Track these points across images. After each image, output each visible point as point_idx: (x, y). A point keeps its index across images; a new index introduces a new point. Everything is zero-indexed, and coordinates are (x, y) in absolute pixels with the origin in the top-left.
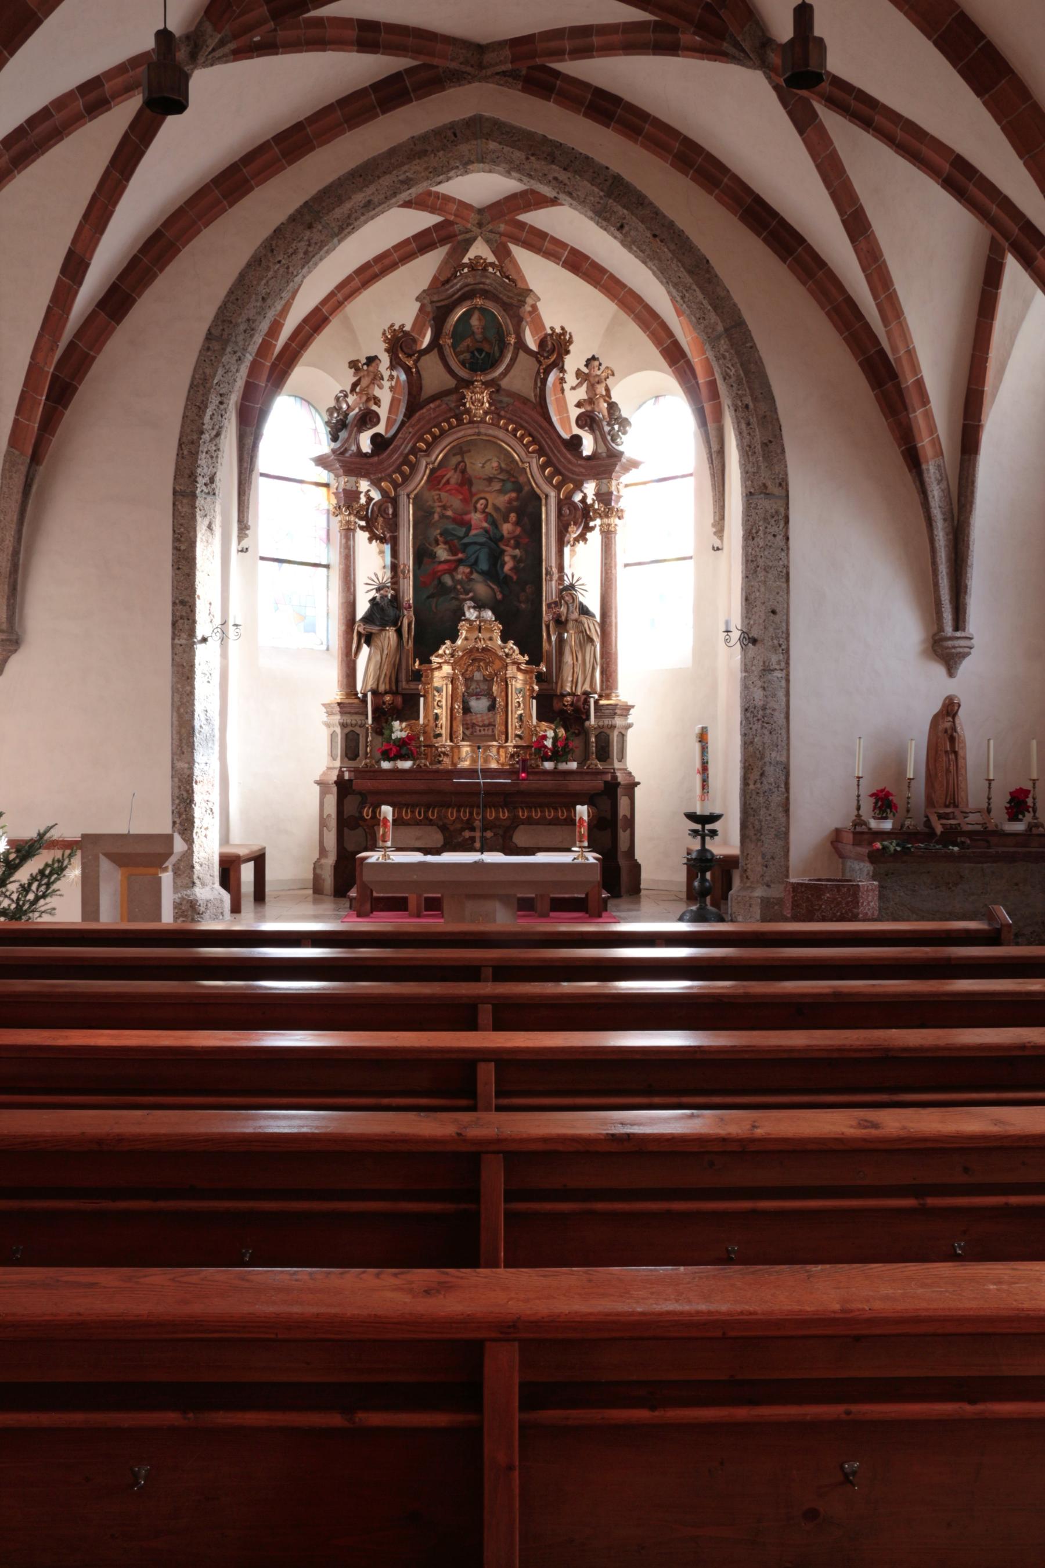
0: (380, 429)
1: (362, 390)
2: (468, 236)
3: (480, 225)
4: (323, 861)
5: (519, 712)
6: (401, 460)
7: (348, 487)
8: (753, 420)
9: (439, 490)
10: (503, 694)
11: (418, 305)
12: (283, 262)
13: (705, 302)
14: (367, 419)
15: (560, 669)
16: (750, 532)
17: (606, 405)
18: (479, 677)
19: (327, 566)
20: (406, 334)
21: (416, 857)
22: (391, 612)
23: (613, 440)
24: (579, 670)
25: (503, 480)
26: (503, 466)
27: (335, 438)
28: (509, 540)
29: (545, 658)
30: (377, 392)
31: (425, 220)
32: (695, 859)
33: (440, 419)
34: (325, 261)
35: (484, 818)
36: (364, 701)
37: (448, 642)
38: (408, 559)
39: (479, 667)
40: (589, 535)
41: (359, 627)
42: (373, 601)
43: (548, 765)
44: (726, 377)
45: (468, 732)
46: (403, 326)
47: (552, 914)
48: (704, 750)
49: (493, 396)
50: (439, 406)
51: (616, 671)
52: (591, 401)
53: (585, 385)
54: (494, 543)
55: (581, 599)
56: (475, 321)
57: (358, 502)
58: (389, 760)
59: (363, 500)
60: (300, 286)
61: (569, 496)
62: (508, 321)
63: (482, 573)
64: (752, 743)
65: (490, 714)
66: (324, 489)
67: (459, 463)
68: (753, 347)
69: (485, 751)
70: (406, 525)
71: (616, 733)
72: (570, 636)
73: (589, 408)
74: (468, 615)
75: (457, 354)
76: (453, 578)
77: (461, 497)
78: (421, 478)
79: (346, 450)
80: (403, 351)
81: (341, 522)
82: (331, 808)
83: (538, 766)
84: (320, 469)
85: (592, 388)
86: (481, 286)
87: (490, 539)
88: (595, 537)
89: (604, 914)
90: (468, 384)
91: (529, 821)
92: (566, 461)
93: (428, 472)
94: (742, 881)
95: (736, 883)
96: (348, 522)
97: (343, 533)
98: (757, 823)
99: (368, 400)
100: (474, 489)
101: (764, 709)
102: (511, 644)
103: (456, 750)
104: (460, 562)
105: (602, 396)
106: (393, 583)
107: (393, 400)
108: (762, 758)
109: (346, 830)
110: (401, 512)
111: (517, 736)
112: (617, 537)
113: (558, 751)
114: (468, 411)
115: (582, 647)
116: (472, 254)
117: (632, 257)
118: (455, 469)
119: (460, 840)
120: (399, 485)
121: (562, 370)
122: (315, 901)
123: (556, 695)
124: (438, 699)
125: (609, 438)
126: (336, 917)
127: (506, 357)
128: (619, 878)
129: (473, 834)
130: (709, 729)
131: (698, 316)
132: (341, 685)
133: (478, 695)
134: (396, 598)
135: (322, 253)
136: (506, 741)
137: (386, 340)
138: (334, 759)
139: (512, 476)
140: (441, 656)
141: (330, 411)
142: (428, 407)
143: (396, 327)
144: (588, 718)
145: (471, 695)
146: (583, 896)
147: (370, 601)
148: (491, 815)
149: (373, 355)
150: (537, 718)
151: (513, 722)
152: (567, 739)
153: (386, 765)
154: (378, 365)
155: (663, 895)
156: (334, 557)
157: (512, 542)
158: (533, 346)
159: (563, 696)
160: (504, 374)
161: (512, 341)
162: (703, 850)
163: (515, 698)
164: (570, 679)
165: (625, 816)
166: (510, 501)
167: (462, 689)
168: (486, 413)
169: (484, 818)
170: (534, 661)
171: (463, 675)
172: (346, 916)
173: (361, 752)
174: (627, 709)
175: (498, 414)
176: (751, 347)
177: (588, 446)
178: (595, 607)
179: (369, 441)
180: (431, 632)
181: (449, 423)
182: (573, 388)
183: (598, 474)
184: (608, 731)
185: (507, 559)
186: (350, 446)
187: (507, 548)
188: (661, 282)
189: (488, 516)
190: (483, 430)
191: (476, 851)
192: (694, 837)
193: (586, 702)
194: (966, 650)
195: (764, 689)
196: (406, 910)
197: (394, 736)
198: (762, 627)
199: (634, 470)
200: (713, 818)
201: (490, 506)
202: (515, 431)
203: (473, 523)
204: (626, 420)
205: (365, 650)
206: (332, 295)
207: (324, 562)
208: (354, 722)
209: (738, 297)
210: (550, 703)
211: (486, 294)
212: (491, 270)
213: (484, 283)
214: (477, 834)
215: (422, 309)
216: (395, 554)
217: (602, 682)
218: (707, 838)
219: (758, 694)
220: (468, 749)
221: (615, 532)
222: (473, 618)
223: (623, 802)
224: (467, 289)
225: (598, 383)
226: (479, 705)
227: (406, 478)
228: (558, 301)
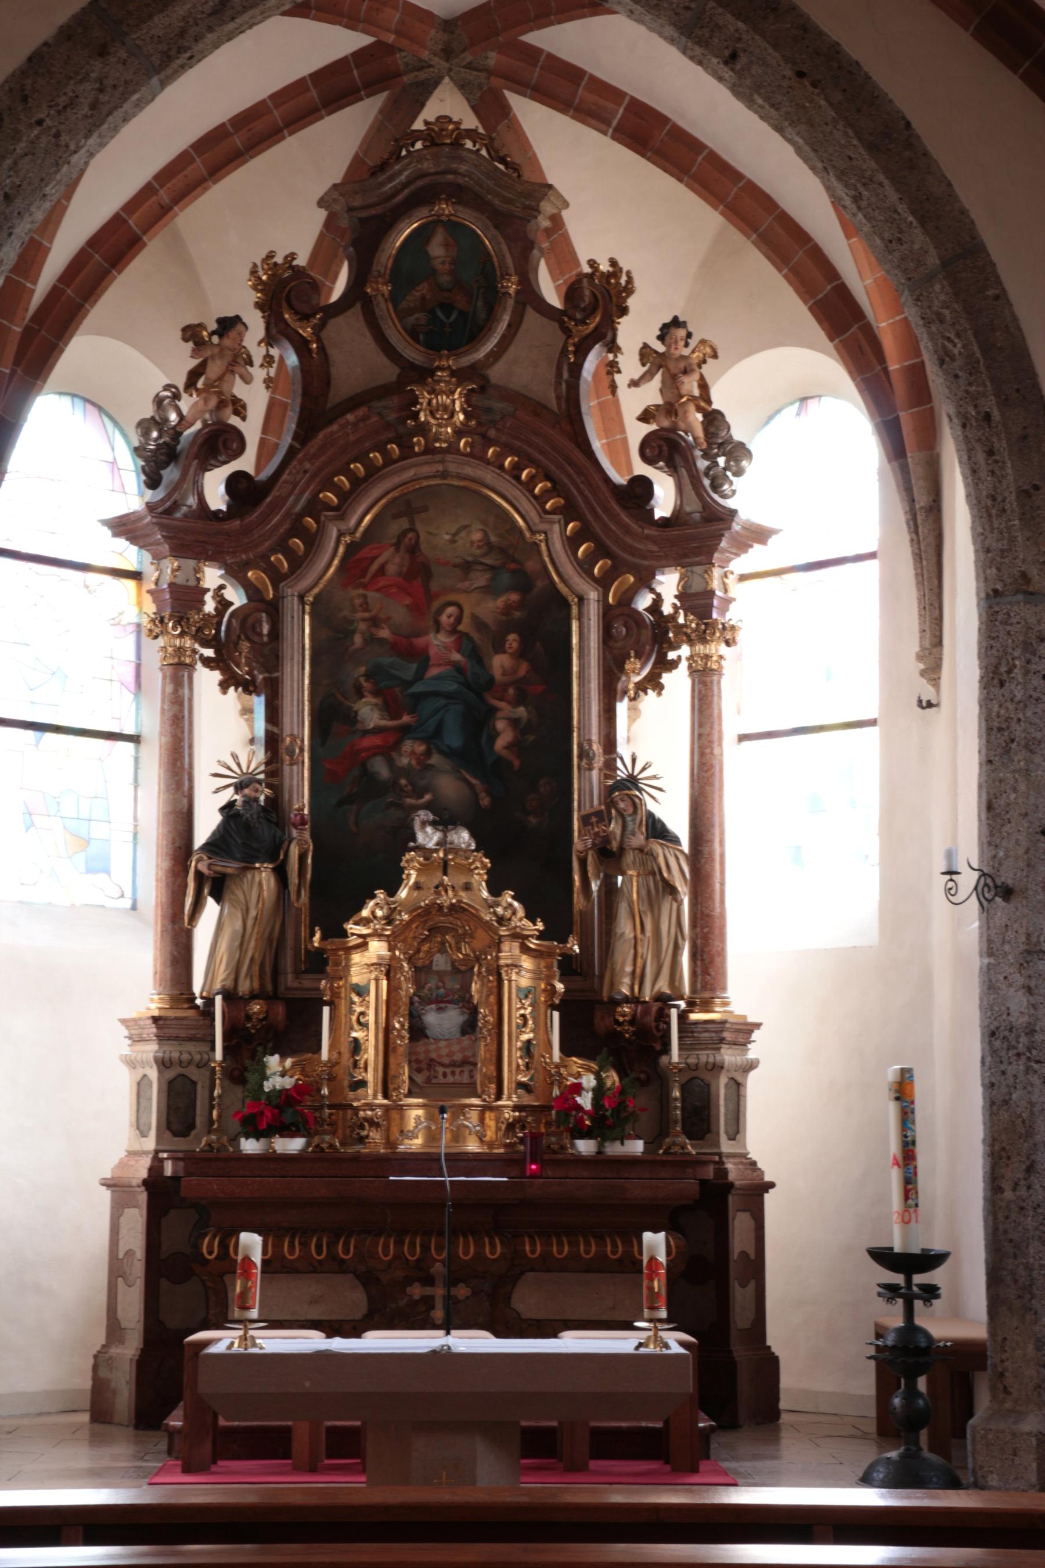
0: (246, 463)
1: (208, 386)
2: (423, 75)
3: (448, 53)
4: (114, 1351)
5: (525, 1037)
6: (287, 526)
7: (180, 580)
8: (1001, 445)
9: (365, 586)
10: (492, 999)
11: (322, 214)
12: (48, 122)
13: (902, 208)
14: (219, 442)
15: (607, 948)
16: (996, 671)
17: (699, 417)
18: (442, 969)
19: (135, 739)
20: (299, 273)
21: (312, 1341)
22: (265, 832)
23: (716, 487)
24: (646, 951)
25: (492, 568)
26: (493, 539)
27: (152, 481)
28: (505, 687)
29: (576, 928)
30: (239, 389)
31: (334, 42)
32: (894, 1347)
33: (367, 444)
34: (134, 122)
35: (452, 1257)
36: (208, 1012)
37: (381, 894)
38: (300, 726)
39: (443, 943)
40: (666, 678)
41: (199, 863)
42: (228, 809)
43: (585, 1147)
44: (944, 359)
45: (419, 1079)
46: (292, 256)
47: (593, 1464)
48: (906, 1116)
49: (474, 399)
50: (364, 419)
51: (722, 953)
52: (670, 408)
53: (658, 377)
54: (475, 694)
55: (651, 806)
56: (437, 249)
57: (200, 610)
58: (257, 1134)
59: (210, 606)
60: (82, 173)
61: (627, 598)
62: (504, 248)
63: (450, 754)
64: (1006, 1102)
65: (466, 1041)
66: (131, 584)
67: (404, 533)
68: (1001, 296)
69: (455, 1117)
70: (297, 657)
71: (723, 1080)
72: (628, 881)
73: (666, 423)
74: (420, 838)
75: (401, 315)
76: (390, 763)
77: (408, 601)
78: (327, 564)
79: (176, 506)
80: (291, 307)
81: (164, 649)
82: (134, 1239)
83: (563, 1148)
84: (122, 543)
85: (671, 383)
86: (450, 177)
87: (467, 685)
88: (678, 683)
89: (703, 1465)
90: (423, 374)
91: (546, 1264)
92: (621, 530)
93: (341, 550)
94: (994, 1397)
95: (983, 1400)
96: (180, 650)
97: (169, 671)
98: (1021, 1271)
99: (221, 405)
100: (434, 586)
101: (1031, 1032)
102: (508, 897)
103: (394, 1115)
104: (405, 731)
105: (692, 399)
106: (269, 774)
107: (272, 405)
108: (1030, 1133)
109: (164, 1283)
110: (287, 632)
111: (521, 1085)
112: (724, 681)
113: (604, 1118)
114: (423, 429)
115: (653, 903)
116: (431, 111)
117: (755, 117)
118: (397, 546)
119: (402, 1303)
120: (284, 577)
121: (613, 347)
122: (96, 1440)
123: (601, 1002)
124: (359, 1009)
125: (707, 482)
126: (137, 1475)
127: (499, 321)
128: (733, 1387)
129: (428, 1291)
130: (916, 1074)
131: (887, 235)
132: (161, 982)
133: (440, 1002)
134: (275, 804)
135: (127, 106)
136: (499, 1096)
137: (258, 285)
138: (144, 1135)
139: (511, 561)
140: (365, 922)
141: (145, 427)
142: (342, 421)
143: (279, 259)
144: (666, 1049)
145: (427, 1001)
146: (659, 1425)
147: (222, 810)
148: (467, 1250)
149: (231, 314)
150: (562, 1049)
151: (512, 1057)
152: (622, 1091)
153: (250, 1146)
154: (241, 337)
155: (828, 1425)
156: (148, 718)
157: (511, 691)
158: (552, 297)
159: (615, 1003)
160: (496, 355)
161: (513, 289)
162: (910, 1329)
163: (517, 1009)
164: (629, 969)
165: (743, 1254)
166: (507, 610)
167: (408, 989)
168: (459, 433)
169: (452, 1257)
170: (556, 931)
171: (410, 960)
172: (160, 1471)
173: (199, 1121)
174: (746, 1030)
175: (484, 436)
176: (997, 298)
177: (665, 499)
178: (679, 824)
179: (222, 489)
180: (348, 870)
181: (385, 453)
182: (634, 384)
183: (686, 556)
184: (707, 1076)
185: (500, 725)
186: (184, 497)
187: (502, 704)
188: (813, 168)
189: (462, 640)
190: (452, 468)
191: (435, 1327)
192: (890, 1300)
193: (663, 1016)
194: (650, 821)
195: (1029, 990)
196: (287, 1456)
197: (267, 1086)
198: (1021, 864)
199: (757, 547)
200: (930, 1260)
201: (466, 620)
202: (517, 468)
203: (432, 652)
204: (741, 445)
205: (211, 909)
206: (147, 191)
207: (130, 730)
208: (185, 1057)
209: (971, 194)
210: (589, 1017)
211: (459, 194)
212: (469, 144)
213: (455, 172)
214: (439, 1292)
215: (329, 224)
216: (273, 715)
217: (694, 974)
218: (918, 1304)
219: (1018, 1002)
220: (420, 1112)
221: (719, 672)
222: (431, 845)
223: (740, 1223)
224: (420, 183)
225: (685, 372)
226: (443, 1022)
227: (298, 563)
228: (604, 206)
